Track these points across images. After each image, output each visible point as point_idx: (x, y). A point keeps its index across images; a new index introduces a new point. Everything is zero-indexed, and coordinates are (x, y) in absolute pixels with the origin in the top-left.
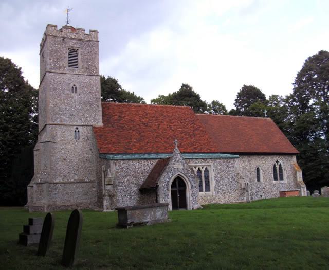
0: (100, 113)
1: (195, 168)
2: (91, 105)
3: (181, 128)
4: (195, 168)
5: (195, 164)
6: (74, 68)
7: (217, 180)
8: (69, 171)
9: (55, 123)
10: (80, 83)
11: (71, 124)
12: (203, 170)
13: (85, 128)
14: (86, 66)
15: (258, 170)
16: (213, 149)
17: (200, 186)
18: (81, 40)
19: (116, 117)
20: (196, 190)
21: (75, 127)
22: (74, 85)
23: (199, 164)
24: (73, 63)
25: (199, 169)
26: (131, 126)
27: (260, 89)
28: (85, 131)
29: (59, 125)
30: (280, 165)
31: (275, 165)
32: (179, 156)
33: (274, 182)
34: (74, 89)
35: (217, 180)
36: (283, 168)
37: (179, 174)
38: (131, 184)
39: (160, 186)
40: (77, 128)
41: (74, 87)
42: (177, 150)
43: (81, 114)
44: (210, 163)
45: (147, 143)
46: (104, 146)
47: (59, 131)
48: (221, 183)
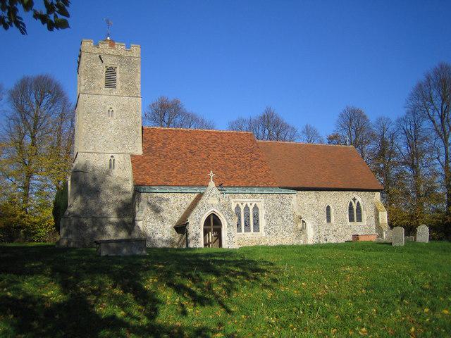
0: (140, 140)
2: (129, 130)
5: (242, 200)
7: (268, 219)
9: (88, 150)
12: (251, 208)
15: (328, 209)
16: (271, 183)
17: (239, 225)
18: (120, 56)
19: (160, 144)
20: (234, 230)
24: (110, 83)
25: (247, 205)
27: (65, 30)
30: (358, 203)
31: (351, 204)
33: (349, 224)
35: (268, 219)
36: (362, 208)
39: (190, 223)
41: (111, 110)
42: (212, 184)
45: (192, 174)
46: (140, 177)
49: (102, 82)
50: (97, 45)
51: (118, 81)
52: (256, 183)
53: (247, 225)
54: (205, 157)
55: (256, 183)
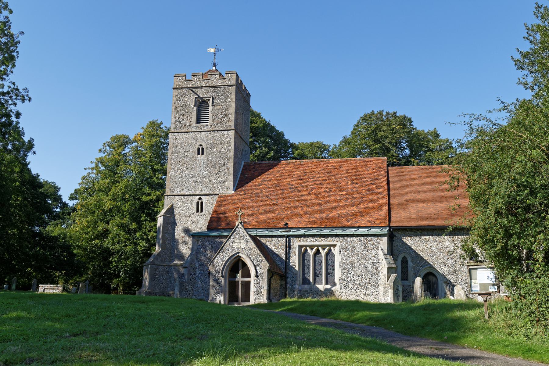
1: (312, 249)
7: (345, 269)
9: (174, 193)
11: (193, 193)
13: (210, 198)
18: (214, 87)
21: (198, 197)
28: (211, 201)
40: (200, 199)
43: (207, 180)
52: (357, 222)
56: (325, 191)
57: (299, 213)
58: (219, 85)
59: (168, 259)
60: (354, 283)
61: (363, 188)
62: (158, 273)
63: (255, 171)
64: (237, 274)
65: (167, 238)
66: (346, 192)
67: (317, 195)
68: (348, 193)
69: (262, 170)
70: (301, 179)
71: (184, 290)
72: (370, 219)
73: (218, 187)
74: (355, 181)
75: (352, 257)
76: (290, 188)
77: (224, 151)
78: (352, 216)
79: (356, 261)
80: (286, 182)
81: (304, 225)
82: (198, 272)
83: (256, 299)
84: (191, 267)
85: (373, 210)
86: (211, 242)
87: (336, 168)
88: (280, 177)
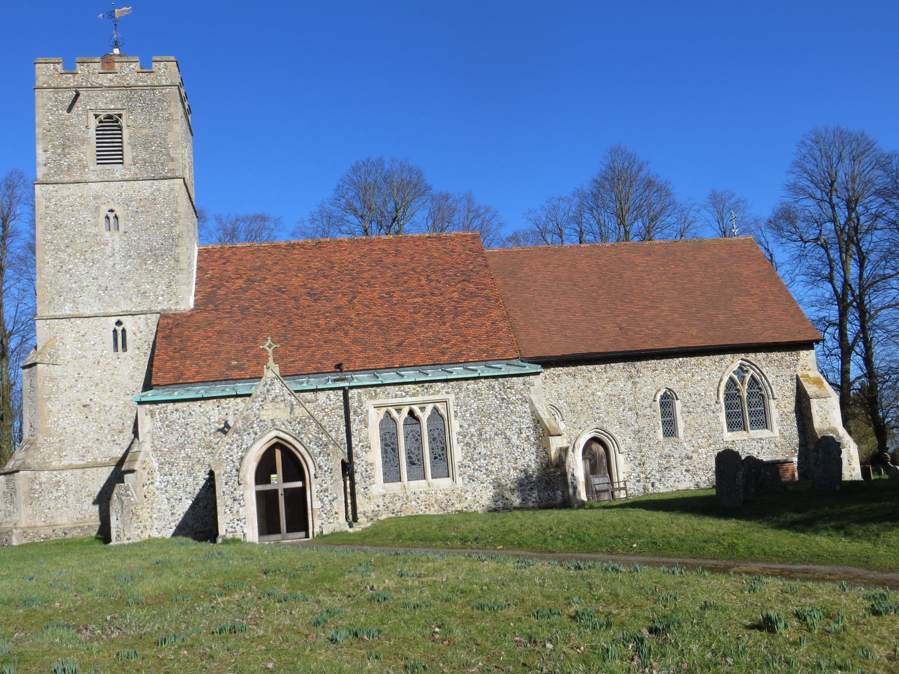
1: (399, 411)
3: (423, 296)
4: (399, 411)
6: (108, 166)
7: (468, 444)
8: (96, 436)
10: (127, 203)
12: (424, 417)
14: (143, 155)
16: (499, 351)
19: (240, 282)
22: (111, 211)
23: (408, 399)
25: (411, 413)
26: (273, 304)
28: (143, 327)
29: (68, 318)
32: (278, 385)
34: (112, 220)
35: (468, 444)
37: (277, 437)
38: (197, 467)
40: (119, 323)
42: (272, 370)
43: (131, 284)
44: (442, 392)
45: (299, 347)
47: (68, 332)
48: (483, 451)
49: (89, 151)
50: (70, 69)
51: (127, 148)
52: (460, 354)
53: (415, 462)
54: (343, 301)
55: (460, 354)
56: (381, 298)
57: (342, 344)
58: (141, 84)
59: (56, 455)
60: (487, 470)
61: (452, 289)
62: (38, 487)
63: (224, 263)
64: (713, 492)
65: (51, 411)
66: (421, 297)
67: (366, 306)
68: (428, 300)
69: (240, 260)
70: (326, 277)
71: (135, 518)
72: (483, 347)
73: (157, 297)
74: (433, 277)
75: (480, 421)
76: (309, 294)
77: (163, 222)
78: (447, 342)
79: (488, 429)
80: (296, 284)
81: (360, 366)
82: (158, 479)
83: (322, 524)
84: (144, 468)
85: (484, 329)
86: (183, 412)
87: (389, 253)
88: (282, 273)
